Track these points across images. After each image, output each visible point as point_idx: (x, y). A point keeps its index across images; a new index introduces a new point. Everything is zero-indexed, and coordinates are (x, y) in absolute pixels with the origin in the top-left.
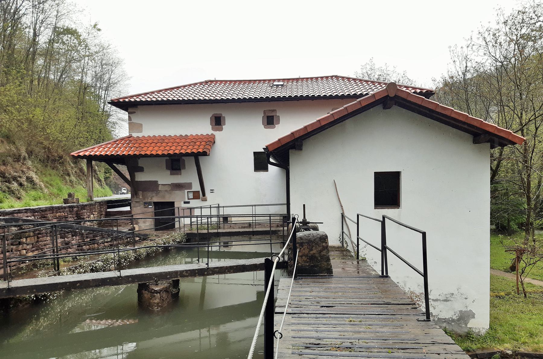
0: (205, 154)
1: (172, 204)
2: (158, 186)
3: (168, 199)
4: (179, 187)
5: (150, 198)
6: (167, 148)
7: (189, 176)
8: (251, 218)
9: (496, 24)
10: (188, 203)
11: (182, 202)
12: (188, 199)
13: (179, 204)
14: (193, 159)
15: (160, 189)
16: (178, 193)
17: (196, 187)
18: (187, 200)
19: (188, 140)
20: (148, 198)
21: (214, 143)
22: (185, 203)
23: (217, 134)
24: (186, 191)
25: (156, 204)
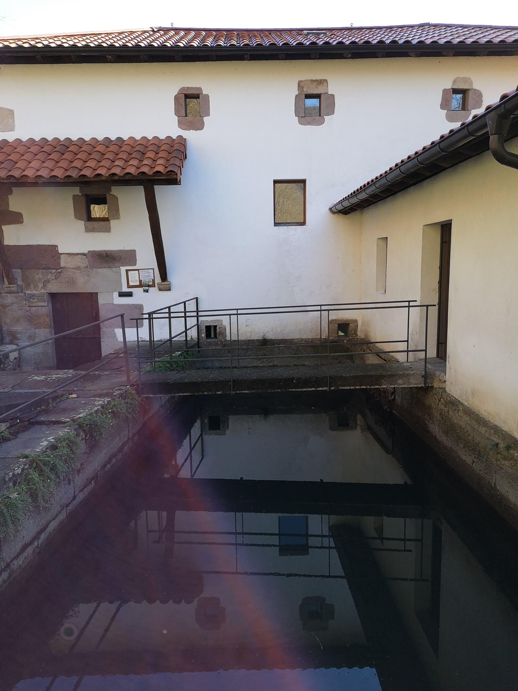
0: (172, 179)
1: (93, 297)
2: (59, 258)
3: (83, 285)
4: (107, 259)
5: (41, 285)
6: (77, 164)
7: (129, 232)
8: (373, 188)
9: (147, 293)
10: (130, 294)
11: (116, 294)
12: (129, 286)
13: (110, 300)
14: (139, 192)
15: (62, 264)
16: (104, 272)
17: (146, 258)
18: (125, 289)
19: (112, 148)
20: (36, 287)
21: (186, 158)
22: (122, 295)
23: (191, 136)
24: (123, 269)
25: (53, 296)
